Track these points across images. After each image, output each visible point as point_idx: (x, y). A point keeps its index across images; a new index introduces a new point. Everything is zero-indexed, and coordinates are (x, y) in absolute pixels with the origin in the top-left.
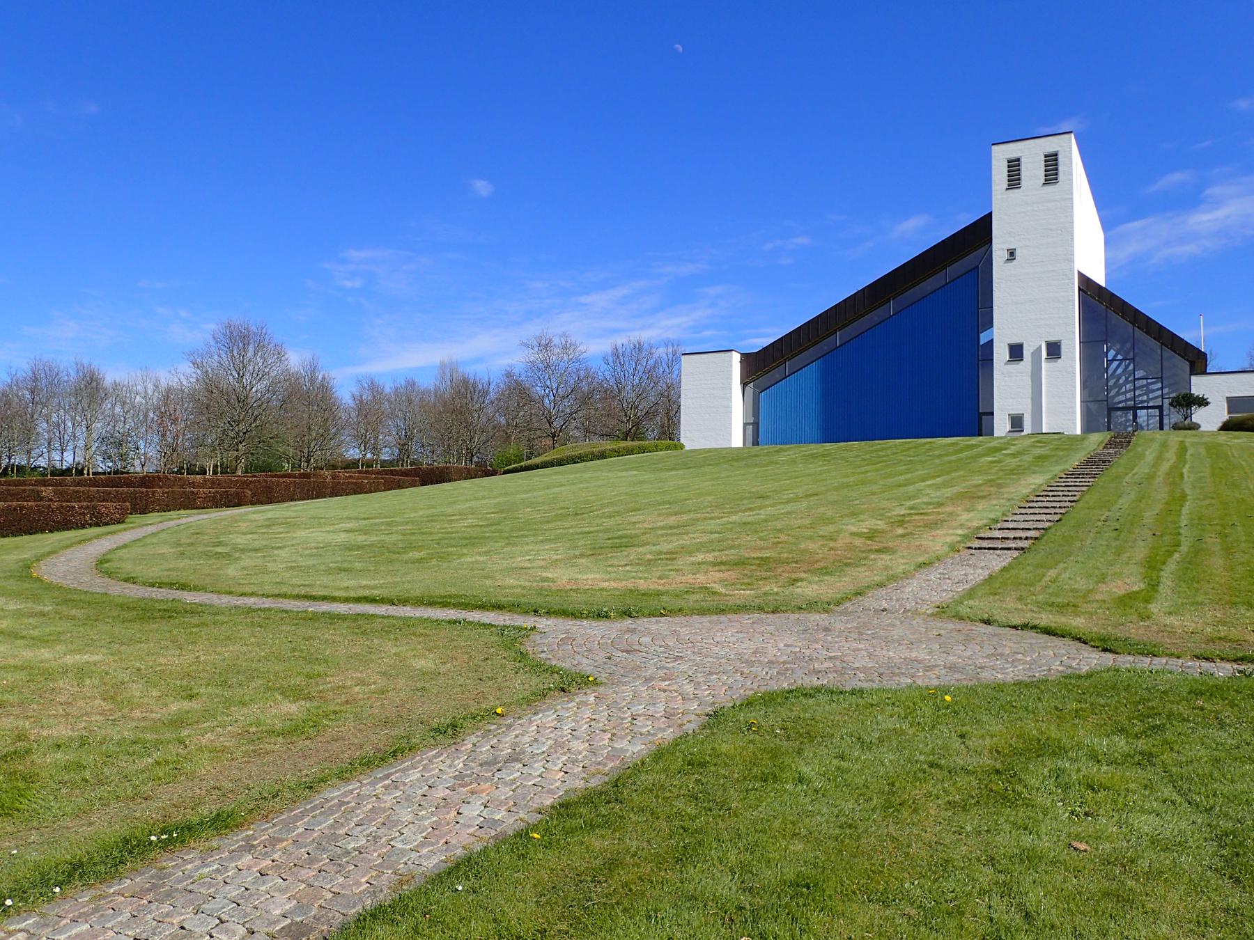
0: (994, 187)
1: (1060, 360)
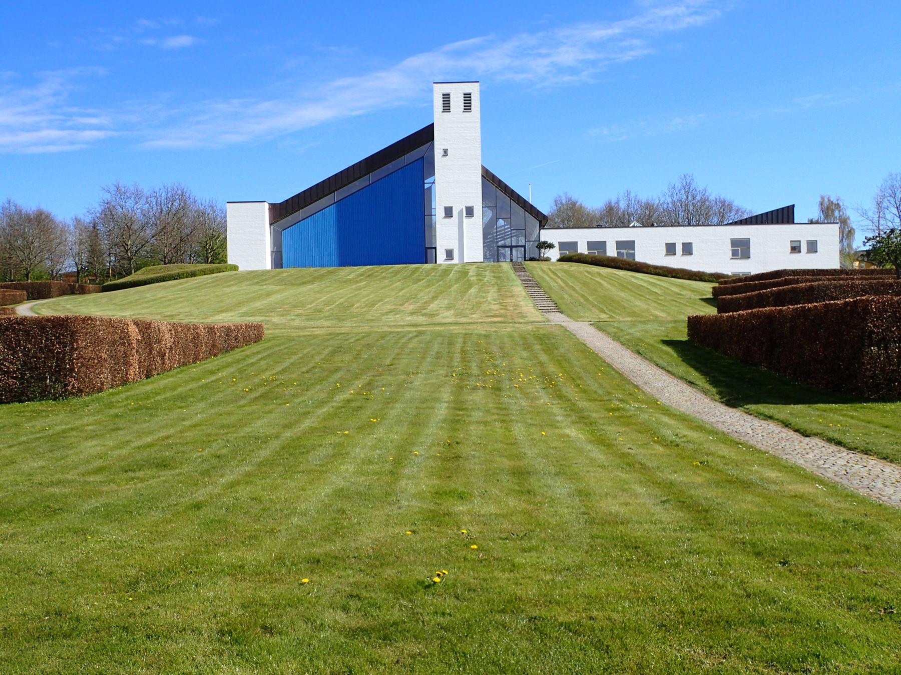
0: (435, 110)
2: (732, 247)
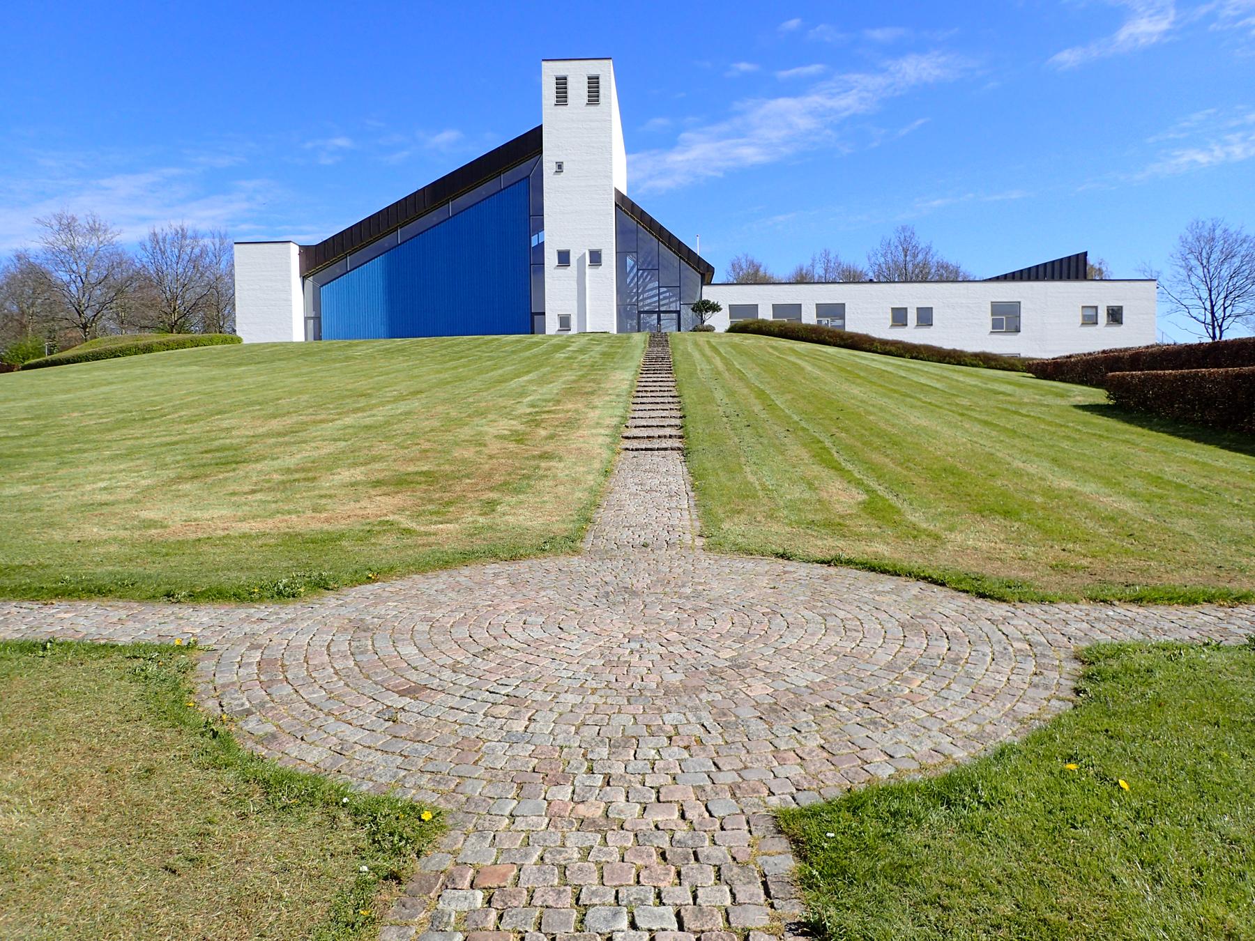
1: (600, 267)
2: (992, 315)
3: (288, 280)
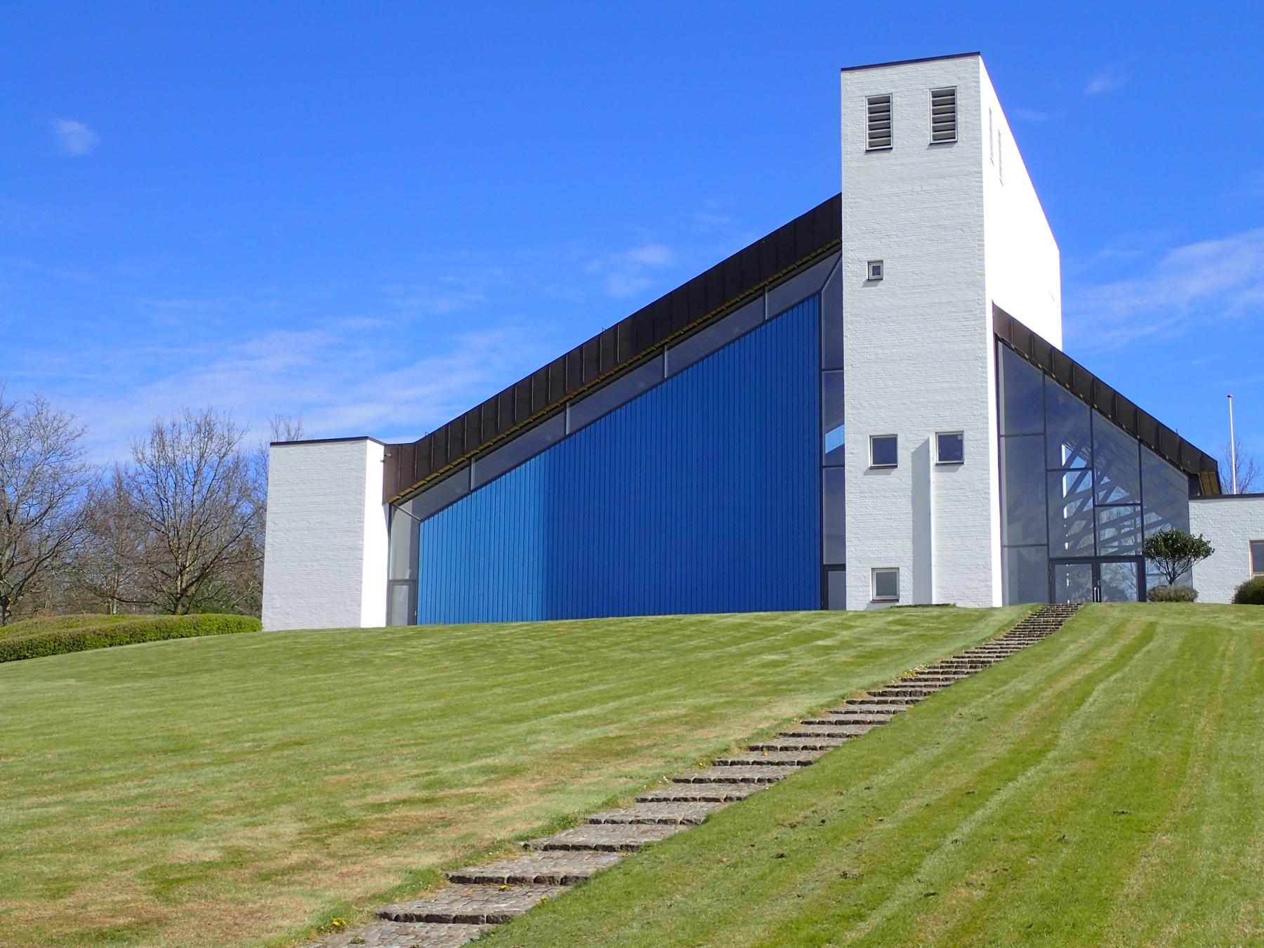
0: (846, 147)
3: (358, 511)
